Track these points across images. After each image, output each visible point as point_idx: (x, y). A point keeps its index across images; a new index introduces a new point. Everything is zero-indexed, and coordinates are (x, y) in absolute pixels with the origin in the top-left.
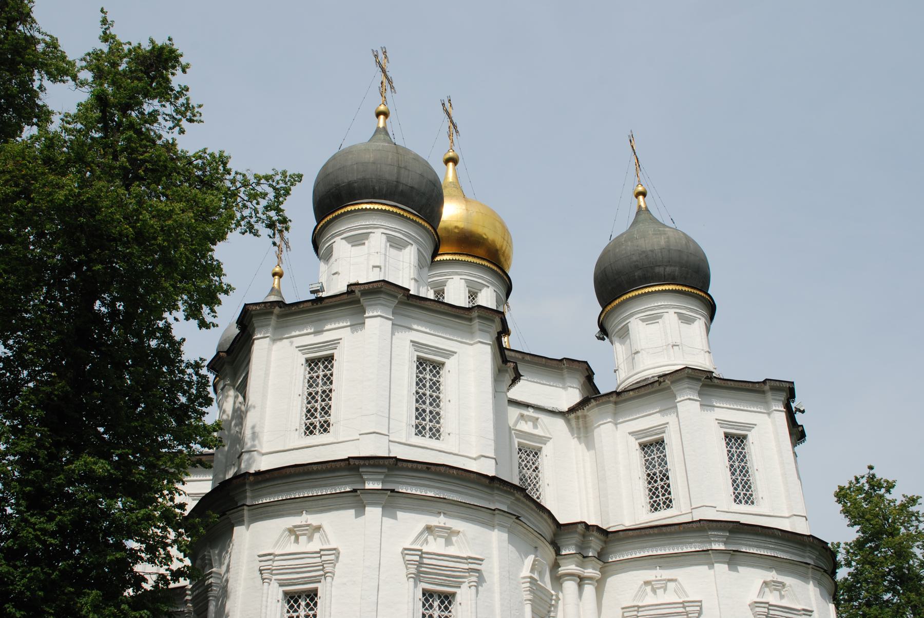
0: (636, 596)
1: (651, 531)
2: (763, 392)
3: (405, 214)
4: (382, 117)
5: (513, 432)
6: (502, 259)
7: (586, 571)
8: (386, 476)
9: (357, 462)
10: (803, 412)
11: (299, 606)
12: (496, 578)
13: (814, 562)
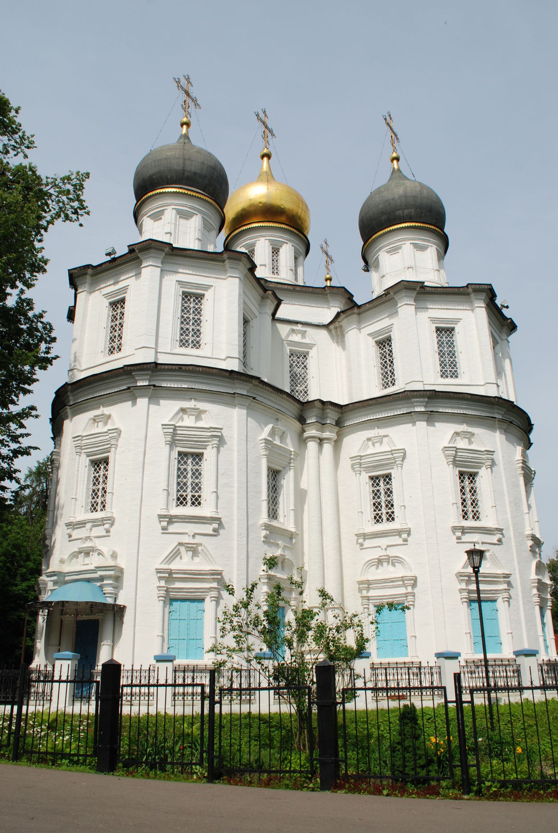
0: (360, 449)
1: (370, 402)
2: (468, 294)
3: (189, 193)
4: (185, 126)
5: (285, 342)
6: (299, 222)
7: (324, 434)
8: (152, 376)
9: (129, 368)
10: (507, 307)
11: (100, 469)
12: (235, 442)
13: (503, 417)
